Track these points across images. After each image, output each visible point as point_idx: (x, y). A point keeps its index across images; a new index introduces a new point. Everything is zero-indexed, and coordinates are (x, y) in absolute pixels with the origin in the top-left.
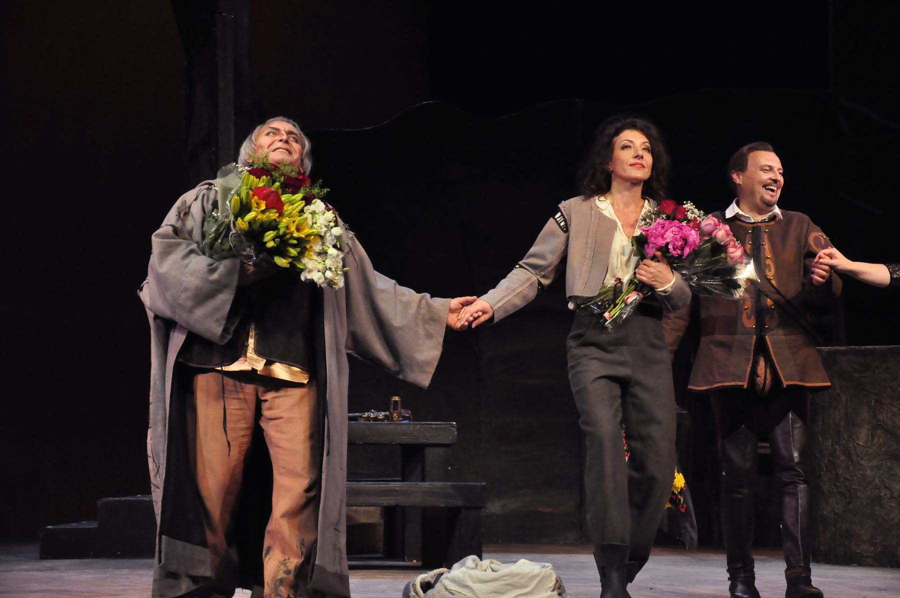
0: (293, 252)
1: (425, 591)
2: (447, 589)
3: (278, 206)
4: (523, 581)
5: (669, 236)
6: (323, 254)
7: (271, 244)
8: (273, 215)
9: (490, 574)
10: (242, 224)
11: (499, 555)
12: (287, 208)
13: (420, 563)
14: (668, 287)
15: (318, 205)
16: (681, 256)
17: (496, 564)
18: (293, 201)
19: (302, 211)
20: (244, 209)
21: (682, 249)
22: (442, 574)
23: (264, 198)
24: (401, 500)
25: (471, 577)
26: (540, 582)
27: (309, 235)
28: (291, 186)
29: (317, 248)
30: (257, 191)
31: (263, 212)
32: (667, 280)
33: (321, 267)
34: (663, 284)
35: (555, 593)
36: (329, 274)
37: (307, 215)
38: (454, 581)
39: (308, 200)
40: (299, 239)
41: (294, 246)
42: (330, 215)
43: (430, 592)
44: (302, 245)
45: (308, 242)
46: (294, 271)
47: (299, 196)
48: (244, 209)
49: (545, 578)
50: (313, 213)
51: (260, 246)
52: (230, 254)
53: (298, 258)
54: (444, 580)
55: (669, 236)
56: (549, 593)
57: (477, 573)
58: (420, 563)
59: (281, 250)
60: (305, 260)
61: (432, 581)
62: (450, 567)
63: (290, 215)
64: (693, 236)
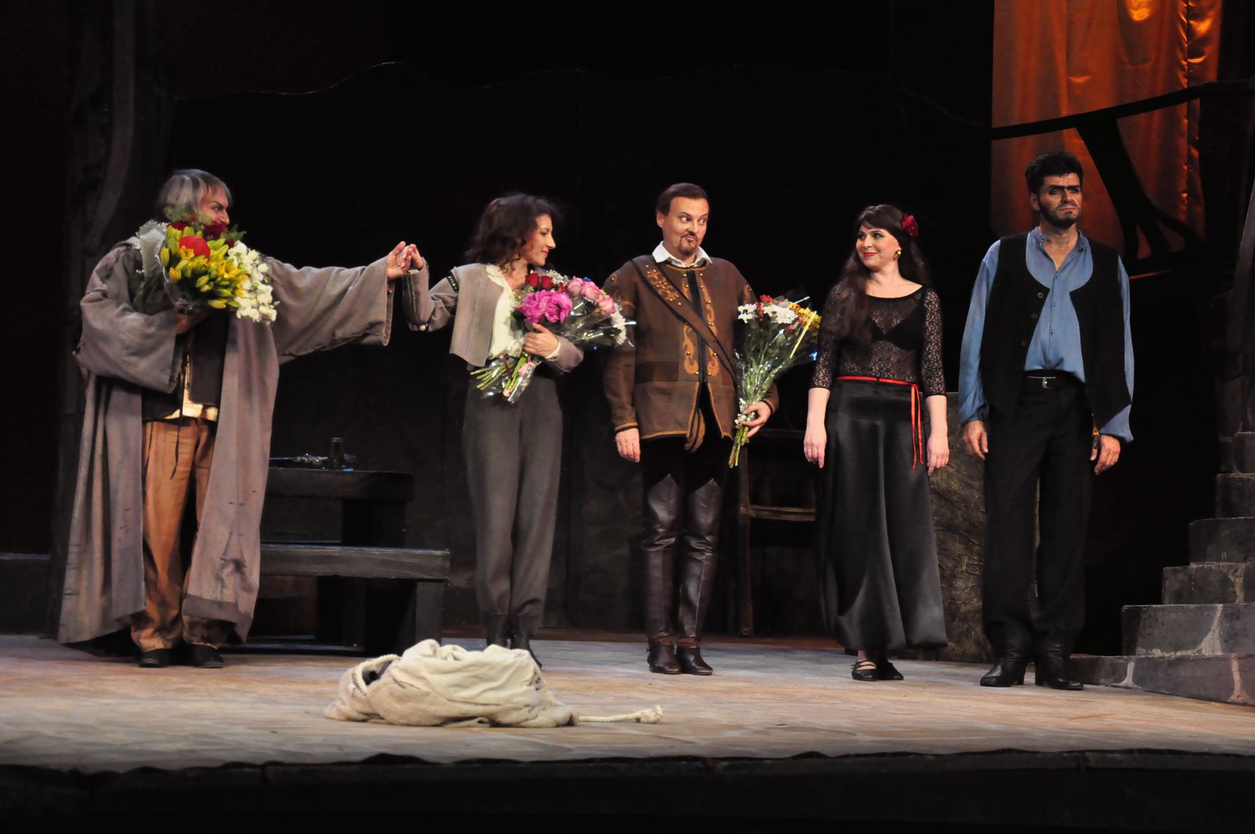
0: (227, 292)
1: (368, 682)
2: (396, 681)
3: (206, 252)
4: (492, 673)
5: (543, 305)
6: (254, 290)
7: (206, 288)
8: (202, 260)
9: (451, 664)
10: (175, 273)
11: (464, 640)
12: (213, 253)
13: (361, 649)
14: (555, 353)
15: (240, 247)
16: (559, 321)
17: (460, 651)
18: (217, 247)
19: (227, 255)
20: (174, 260)
21: (559, 314)
22: (390, 662)
23: (188, 247)
24: (343, 570)
25: (427, 666)
26: (515, 672)
27: (238, 275)
28: (212, 231)
29: (247, 285)
30: (185, 242)
31: (192, 259)
32: (553, 347)
33: (254, 302)
34: (550, 351)
35: (533, 687)
36: (263, 310)
37: (232, 257)
38: (405, 671)
39: (231, 244)
40: (231, 280)
41: (226, 287)
42: (254, 254)
43: (374, 684)
44: (233, 285)
45: (238, 282)
46: (229, 312)
47: (222, 241)
48: (174, 260)
49: (520, 669)
50: (238, 255)
51: (196, 293)
52: (167, 306)
53: (231, 298)
54: (393, 670)
55: (543, 305)
56: (525, 687)
57: (437, 662)
58: (361, 649)
59: (213, 295)
60: (238, 299)
61: (378, 670)
62: (400, 654)
63: (217, 260)
64: (564, 299)
